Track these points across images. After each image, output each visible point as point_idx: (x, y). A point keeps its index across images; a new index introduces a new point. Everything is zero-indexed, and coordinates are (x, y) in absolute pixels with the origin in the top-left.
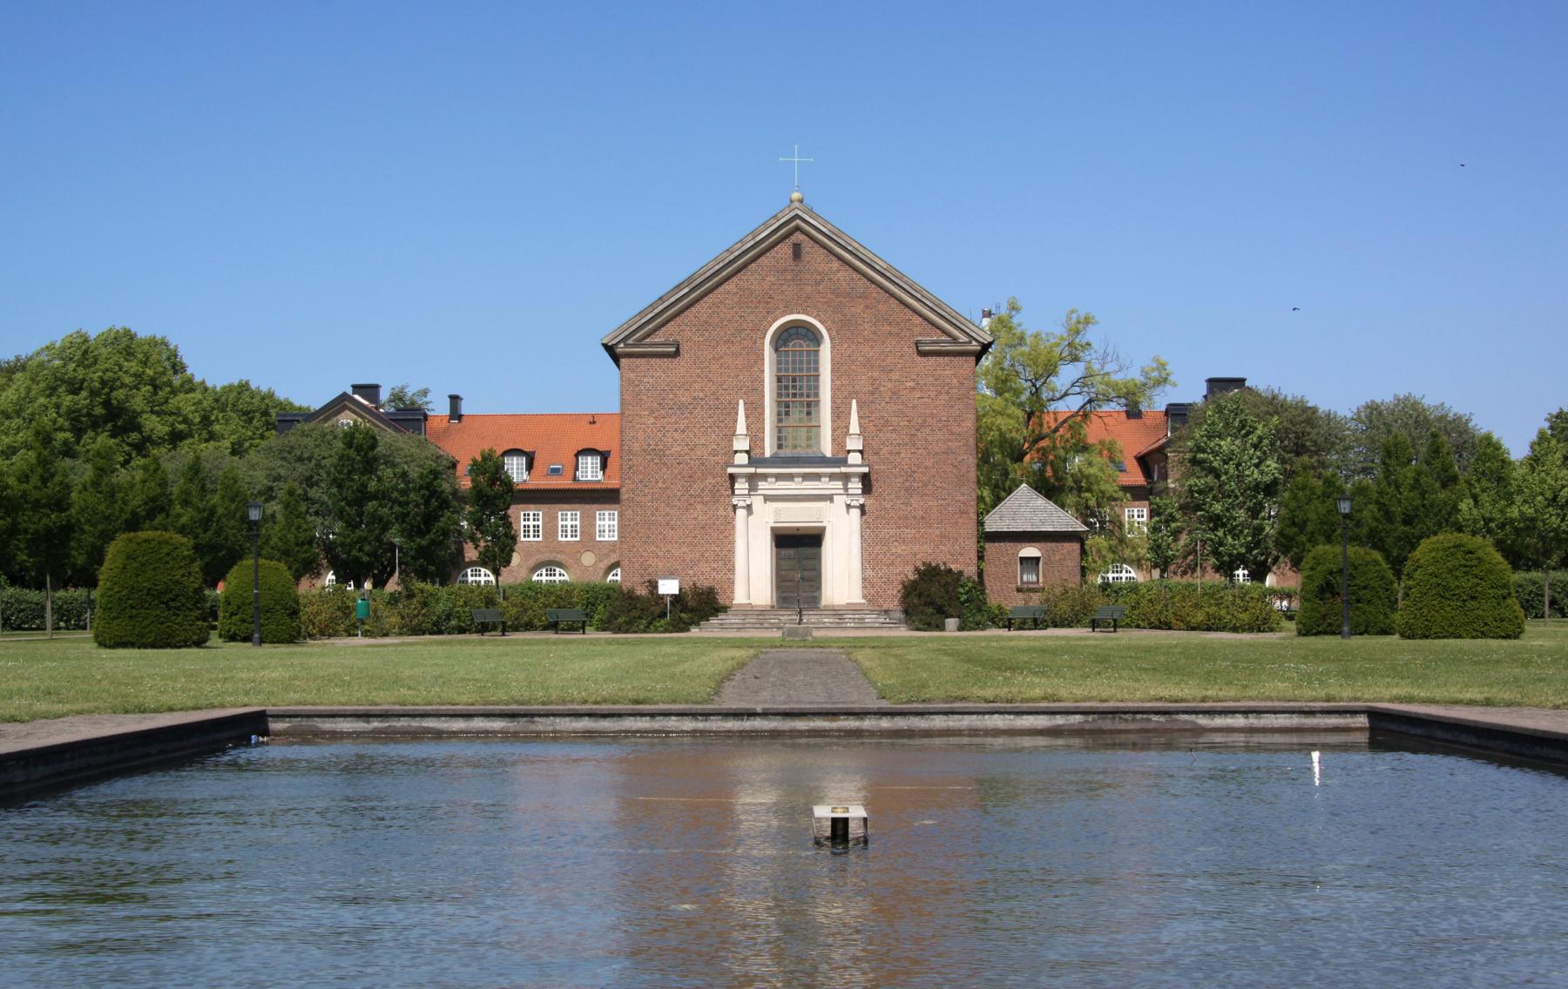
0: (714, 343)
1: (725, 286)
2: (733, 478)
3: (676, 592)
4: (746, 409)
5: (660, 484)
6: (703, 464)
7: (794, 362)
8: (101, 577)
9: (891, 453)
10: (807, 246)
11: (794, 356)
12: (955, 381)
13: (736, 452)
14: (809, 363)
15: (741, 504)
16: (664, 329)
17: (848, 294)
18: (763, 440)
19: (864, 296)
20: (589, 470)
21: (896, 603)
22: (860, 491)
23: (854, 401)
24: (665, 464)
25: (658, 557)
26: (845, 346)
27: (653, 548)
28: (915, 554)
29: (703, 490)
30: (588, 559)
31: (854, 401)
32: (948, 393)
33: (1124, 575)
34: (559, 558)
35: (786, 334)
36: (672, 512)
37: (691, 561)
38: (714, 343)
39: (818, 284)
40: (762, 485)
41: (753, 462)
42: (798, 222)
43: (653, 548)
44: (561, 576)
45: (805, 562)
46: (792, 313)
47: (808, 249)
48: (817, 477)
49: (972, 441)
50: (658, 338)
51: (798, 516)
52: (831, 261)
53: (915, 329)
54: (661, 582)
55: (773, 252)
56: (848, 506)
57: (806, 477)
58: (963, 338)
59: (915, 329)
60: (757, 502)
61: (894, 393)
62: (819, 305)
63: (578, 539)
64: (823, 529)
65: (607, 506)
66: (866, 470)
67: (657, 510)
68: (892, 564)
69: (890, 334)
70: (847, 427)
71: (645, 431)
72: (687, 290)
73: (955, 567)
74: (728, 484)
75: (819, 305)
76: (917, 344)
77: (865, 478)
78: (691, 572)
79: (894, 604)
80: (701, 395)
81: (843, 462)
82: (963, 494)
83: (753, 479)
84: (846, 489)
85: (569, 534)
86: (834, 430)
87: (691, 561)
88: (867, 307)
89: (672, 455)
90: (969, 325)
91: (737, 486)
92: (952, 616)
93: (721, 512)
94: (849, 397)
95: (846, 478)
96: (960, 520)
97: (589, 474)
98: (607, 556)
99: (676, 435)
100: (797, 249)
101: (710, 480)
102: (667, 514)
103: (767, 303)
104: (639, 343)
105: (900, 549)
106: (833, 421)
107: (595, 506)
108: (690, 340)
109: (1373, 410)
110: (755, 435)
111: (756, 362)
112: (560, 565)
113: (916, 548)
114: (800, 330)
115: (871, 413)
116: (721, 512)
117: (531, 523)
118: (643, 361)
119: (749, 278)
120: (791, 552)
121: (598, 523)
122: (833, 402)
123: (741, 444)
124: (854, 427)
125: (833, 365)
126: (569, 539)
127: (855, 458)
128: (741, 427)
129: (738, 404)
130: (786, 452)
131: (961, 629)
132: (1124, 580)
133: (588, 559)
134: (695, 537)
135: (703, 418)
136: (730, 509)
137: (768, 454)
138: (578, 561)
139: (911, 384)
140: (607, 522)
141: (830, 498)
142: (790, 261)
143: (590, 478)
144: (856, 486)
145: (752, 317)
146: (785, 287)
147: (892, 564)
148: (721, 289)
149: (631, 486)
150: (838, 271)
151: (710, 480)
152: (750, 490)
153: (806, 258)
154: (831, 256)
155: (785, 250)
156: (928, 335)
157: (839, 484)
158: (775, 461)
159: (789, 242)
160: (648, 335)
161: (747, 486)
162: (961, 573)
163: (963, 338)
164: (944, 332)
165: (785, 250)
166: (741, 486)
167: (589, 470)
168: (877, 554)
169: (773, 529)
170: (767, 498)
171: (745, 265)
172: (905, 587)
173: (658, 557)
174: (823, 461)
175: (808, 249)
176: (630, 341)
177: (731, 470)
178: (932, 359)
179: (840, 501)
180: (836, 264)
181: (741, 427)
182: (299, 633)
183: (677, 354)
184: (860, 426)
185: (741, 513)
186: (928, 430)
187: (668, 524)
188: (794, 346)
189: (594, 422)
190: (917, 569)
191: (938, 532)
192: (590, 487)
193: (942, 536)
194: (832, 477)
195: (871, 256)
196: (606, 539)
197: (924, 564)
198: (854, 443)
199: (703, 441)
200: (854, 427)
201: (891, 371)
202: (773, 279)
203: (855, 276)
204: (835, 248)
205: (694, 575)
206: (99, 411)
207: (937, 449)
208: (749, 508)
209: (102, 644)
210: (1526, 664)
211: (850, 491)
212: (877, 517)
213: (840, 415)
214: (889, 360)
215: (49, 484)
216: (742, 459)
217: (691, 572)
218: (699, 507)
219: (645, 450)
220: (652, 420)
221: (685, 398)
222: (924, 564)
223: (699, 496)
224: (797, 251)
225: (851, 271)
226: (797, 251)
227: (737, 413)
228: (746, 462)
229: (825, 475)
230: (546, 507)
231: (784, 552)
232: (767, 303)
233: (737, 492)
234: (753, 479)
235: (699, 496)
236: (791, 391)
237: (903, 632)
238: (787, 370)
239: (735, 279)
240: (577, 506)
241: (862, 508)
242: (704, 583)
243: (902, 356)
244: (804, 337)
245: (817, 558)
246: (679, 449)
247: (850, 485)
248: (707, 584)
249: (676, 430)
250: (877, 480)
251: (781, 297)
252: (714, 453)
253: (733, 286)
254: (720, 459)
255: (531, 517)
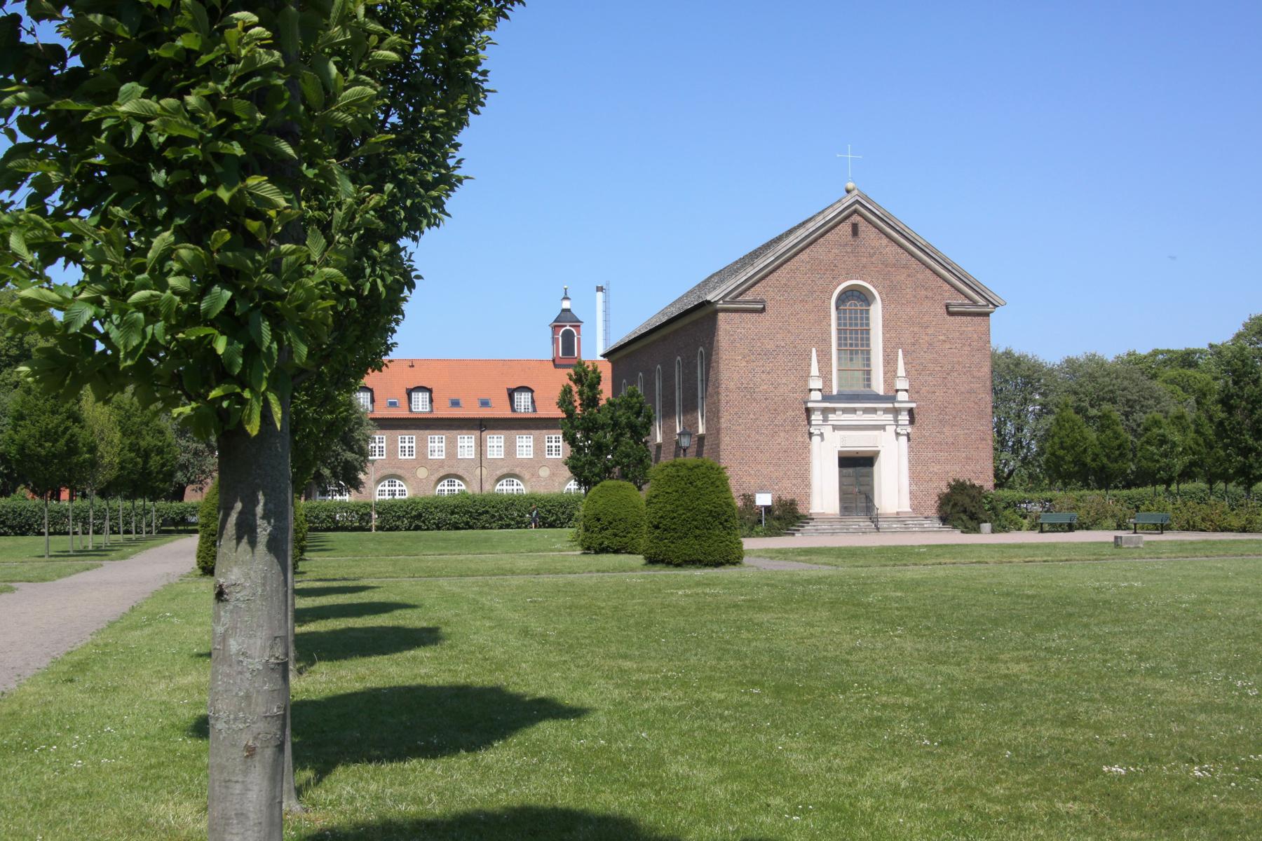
0: (791, 302)
1: (800, 256)
2: (808, 411)
3: (769, 503)
4: (818, 356)
5: (751, 416)
6: (784, 400)
7: (851, 318)
9: (928, 392)
10: (863, 226)
11: (850, 313)
12: (975, 336)
14: (862, 319)
15: (817, 432)
16: (752, 290)
17: (894, 265)
18: (831, 381)
19: (906, 267)
20: (420, 403)
21: (934, 511)
22: (907, 422)
23: (900, 351)
24: (755, 399)
25: (750, 475)
27: (746, 468)
28: (948, 472)
29: (785, 421)
30: (422, 473)
32: (970, 345)
33: (456, 488)
34: (399, 472)
35: (850, 293)
37: (777, 478)
38: (791, 302)
39: (871, 256)
40: (831, 416)
41: (826, 398)
42: (857, 206)
43: (746, 468)
44: (458, 487)
45: (861, 479)
46: (852, 279)
47: (863, 228)
48: (874, 410)
49: (988, 383)
50: (749, 296)
51: (858, 442)
52: (881, 238)
54: (758, 496)
55: (837, 229)
56: (898, 434)
57: (866, 411)
58: (982, 302)
60: (827, 430)
61: (930, 344)
62: (873, 273)
63: (414, 457)
64: (877, 453)
65: (437, 432)
66: (913, 405)
67: (749, 436)
68: (931, 480)
69: (927, 297)
70: (895, 371)
71: (738, 372)
72: (772, 258)
73: (977, 483)
74: (804, 416)
75: (873, 273)
76: (947, 306)
77: (911, 411)
78: (776, 487)
79: (932, 512)
80: (783, 344)
81: (892, 399)
82: (982, 425)
83: (825, 411)
84: (896, 420)
85: (407, 453)
86: (885, 373)
87: (777, 478)
88: (909, 276)
89: (760, 392)
91: (813, 417)
92: (986, 522)
93: (800, 439)
95: (896, 412)
96: (980, 446)
97: (420, 407)
98: (437, 470)
99: (763, 376)
100: (855, 228)
101: (791, 413)
102: (757, 440)
103: (833, 270)
104: (733, 301)
105: (936, 468)
106: (884, 366)
107: (427, 432)
108: (773, 299)
109: (1070, 362)
110: (825, 377)
111: (824, 318)
112: (400, 478)
113: (948, 468)
114: (855, 293)
115: (913, 360)
116: (800, 439)
117: (554, 444)
118: (737, 315)
119: (818, 250)
120: (850, 470)
121: (430, 445)
122: (884, 351)
123: (816, 383)
124: (901, 371)
125: (884, 321)
126: (407, 457)
127: (902, 396)
128: (814, 370)
129: (811, 351)
130: (847, 390)
131: (993, 531)
132: (446, 492)
133: (422, 473)
134: (779, 459)
135: (784, 362)
136: (807, 436)
137: (835, 392)
138: (414, 475)
140: (437, 444)
141: (883, 428)
142: (850, 238)
143: (420, 410)
144: (904, 418)
145: (821, 281)
146: (846, 258)
147: (931, 480)
148: (796, 258)
150: (887, 246)
151: (791, 413)
152: (823, 421)
153: (861, 234)
155: (846, 228)
157: (890, 417)
158: (842, 397)
159: (849, 222)
160: (741, 294)
161: (821, 418)
162: (981, 487)
163: (982, 302)
164: (967, 297)
165: (846, 228)
166: (816, 418)
167: (420, 403)
168: (919, 473)
169: (839, 452)
170: (835, 428)
171: (815, 240)
172: (940, 499)
173: (750, 475)
174: (877, 398)
175: (863, 228)
176: (727, 299)
178: (958, 318)
179: (891, 430)
180: (885, 241)
181: (814, 370)
183: (763, 310)
184: (906, 371)
185: (816, 439)
186: (955, 374)
187: (758, 448)
188: (851, 305)
189: (413, 366)
190: (949, 485)
191: (964, 455)
192: (420, 416)
193: (967, 458)
194: (886, 411)
195: (914, 235)
196: (436, 457)
197: (954, 480)
198: (902, 384)
199: (784, 381)
200: (901, 371)
201: (928, 327)
202: (837, 251)
203: (900, 250)
204: (887, 227)
205: (779, 490)
206: (14, 352)
207: (963, 389)
208: (821, 435)
209: (588, 549)
211: (900, 423)
212: (919, 443)
213: (889, 361)
214: (926, 318)
215: (1219, 406)
216: (816, 396)
217: (776, 487)
218: (782, 434)
219: (739, 388)
220: (744, 364)
221: (770, 346)
222: (954, 480)
223: (782, 425)
224: (855, 230)
225: (897, 247)
226: (855, 230)
227: (810, 359)
228: (820, 398)
229: (880, 409)
230: (388, 432)
231: (845, 471)
232: (833, 270)
233: (813, 423)
234: (825, 411)
235: (782, 425)
236: (849, 342)
237: (955, 537)
238: (845, 325)
239: (808, 251)
240: (413, 431)
241: (908, 435)
242: (787, 496)
243: (936, 315)
244: (859, 298)
245: (871, 475)
246: (765, 387)
247: (900, 417)
248: (789, 497)
249: (763, 372)
250: (918, 414)
252: (793, 391)
253: (806, 255)
254: (799, 396)
255: (407, 440)
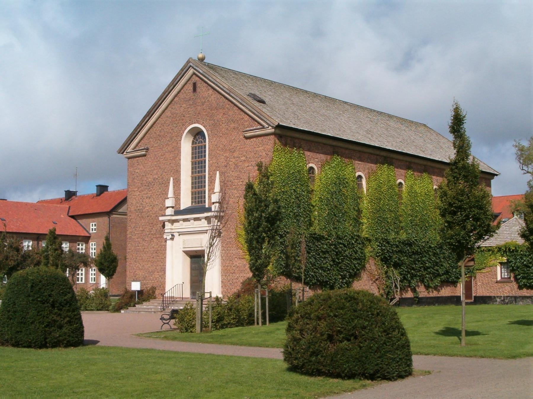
8: (403, 196)
13: (168, 207)
23: (218, 172)
26: (215, 139)
31: (218, 172)
36: (145, 244)
53: (245, 123)
59: (245, 123)
90: (270, 119)
94: (215, 171)
100: (195, 85)
123: (169, 202)
128: (171, 194)
139: (243, 158)
149: (131, 230)
153: (198, 90)
154: (209, 87)
156: (252, 126)
164: (259, 123)
177: (161, 218)
180: (211, 91)
181: (171, 194)
182: (108, 307)
203: (219, 96)
210: (212, 338)
251: (188, 115)
253: (170, 109)
